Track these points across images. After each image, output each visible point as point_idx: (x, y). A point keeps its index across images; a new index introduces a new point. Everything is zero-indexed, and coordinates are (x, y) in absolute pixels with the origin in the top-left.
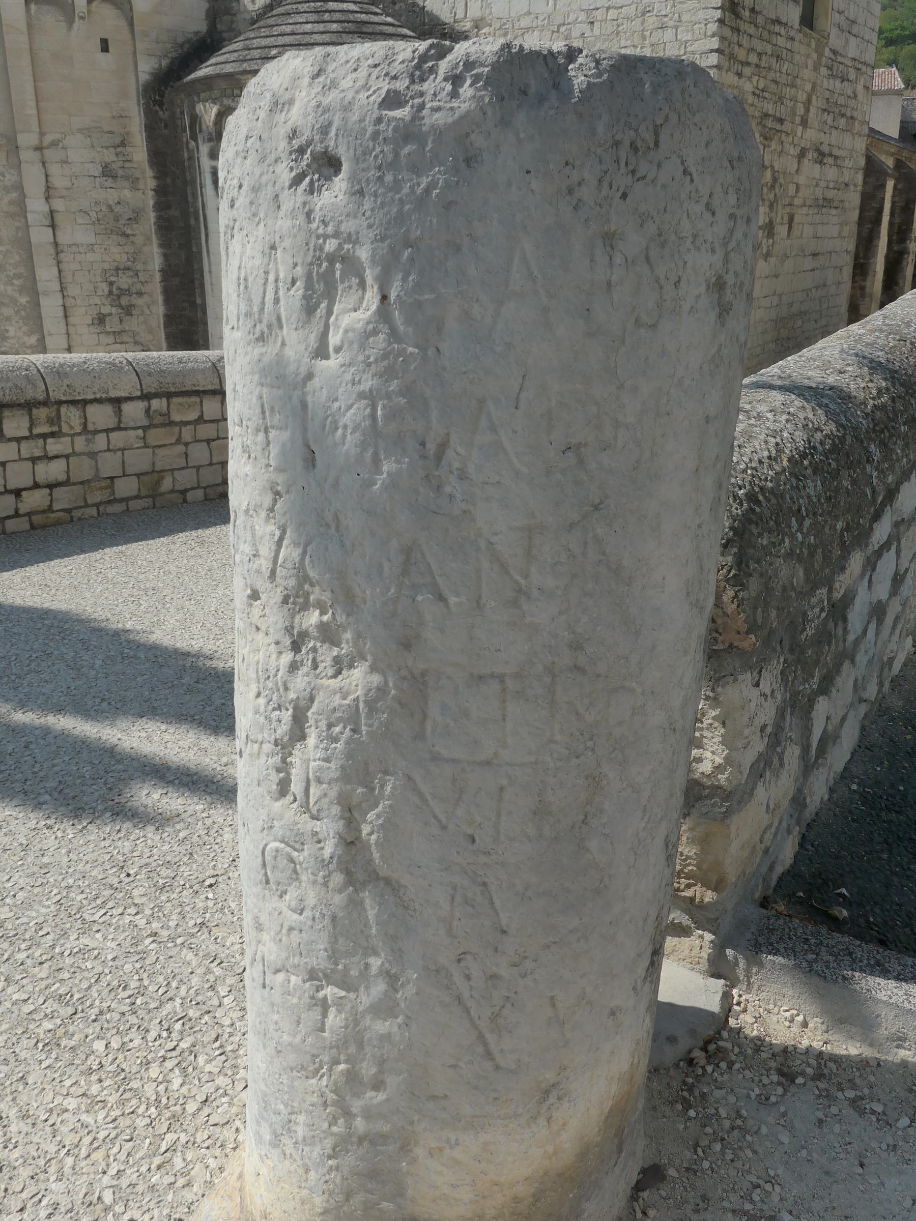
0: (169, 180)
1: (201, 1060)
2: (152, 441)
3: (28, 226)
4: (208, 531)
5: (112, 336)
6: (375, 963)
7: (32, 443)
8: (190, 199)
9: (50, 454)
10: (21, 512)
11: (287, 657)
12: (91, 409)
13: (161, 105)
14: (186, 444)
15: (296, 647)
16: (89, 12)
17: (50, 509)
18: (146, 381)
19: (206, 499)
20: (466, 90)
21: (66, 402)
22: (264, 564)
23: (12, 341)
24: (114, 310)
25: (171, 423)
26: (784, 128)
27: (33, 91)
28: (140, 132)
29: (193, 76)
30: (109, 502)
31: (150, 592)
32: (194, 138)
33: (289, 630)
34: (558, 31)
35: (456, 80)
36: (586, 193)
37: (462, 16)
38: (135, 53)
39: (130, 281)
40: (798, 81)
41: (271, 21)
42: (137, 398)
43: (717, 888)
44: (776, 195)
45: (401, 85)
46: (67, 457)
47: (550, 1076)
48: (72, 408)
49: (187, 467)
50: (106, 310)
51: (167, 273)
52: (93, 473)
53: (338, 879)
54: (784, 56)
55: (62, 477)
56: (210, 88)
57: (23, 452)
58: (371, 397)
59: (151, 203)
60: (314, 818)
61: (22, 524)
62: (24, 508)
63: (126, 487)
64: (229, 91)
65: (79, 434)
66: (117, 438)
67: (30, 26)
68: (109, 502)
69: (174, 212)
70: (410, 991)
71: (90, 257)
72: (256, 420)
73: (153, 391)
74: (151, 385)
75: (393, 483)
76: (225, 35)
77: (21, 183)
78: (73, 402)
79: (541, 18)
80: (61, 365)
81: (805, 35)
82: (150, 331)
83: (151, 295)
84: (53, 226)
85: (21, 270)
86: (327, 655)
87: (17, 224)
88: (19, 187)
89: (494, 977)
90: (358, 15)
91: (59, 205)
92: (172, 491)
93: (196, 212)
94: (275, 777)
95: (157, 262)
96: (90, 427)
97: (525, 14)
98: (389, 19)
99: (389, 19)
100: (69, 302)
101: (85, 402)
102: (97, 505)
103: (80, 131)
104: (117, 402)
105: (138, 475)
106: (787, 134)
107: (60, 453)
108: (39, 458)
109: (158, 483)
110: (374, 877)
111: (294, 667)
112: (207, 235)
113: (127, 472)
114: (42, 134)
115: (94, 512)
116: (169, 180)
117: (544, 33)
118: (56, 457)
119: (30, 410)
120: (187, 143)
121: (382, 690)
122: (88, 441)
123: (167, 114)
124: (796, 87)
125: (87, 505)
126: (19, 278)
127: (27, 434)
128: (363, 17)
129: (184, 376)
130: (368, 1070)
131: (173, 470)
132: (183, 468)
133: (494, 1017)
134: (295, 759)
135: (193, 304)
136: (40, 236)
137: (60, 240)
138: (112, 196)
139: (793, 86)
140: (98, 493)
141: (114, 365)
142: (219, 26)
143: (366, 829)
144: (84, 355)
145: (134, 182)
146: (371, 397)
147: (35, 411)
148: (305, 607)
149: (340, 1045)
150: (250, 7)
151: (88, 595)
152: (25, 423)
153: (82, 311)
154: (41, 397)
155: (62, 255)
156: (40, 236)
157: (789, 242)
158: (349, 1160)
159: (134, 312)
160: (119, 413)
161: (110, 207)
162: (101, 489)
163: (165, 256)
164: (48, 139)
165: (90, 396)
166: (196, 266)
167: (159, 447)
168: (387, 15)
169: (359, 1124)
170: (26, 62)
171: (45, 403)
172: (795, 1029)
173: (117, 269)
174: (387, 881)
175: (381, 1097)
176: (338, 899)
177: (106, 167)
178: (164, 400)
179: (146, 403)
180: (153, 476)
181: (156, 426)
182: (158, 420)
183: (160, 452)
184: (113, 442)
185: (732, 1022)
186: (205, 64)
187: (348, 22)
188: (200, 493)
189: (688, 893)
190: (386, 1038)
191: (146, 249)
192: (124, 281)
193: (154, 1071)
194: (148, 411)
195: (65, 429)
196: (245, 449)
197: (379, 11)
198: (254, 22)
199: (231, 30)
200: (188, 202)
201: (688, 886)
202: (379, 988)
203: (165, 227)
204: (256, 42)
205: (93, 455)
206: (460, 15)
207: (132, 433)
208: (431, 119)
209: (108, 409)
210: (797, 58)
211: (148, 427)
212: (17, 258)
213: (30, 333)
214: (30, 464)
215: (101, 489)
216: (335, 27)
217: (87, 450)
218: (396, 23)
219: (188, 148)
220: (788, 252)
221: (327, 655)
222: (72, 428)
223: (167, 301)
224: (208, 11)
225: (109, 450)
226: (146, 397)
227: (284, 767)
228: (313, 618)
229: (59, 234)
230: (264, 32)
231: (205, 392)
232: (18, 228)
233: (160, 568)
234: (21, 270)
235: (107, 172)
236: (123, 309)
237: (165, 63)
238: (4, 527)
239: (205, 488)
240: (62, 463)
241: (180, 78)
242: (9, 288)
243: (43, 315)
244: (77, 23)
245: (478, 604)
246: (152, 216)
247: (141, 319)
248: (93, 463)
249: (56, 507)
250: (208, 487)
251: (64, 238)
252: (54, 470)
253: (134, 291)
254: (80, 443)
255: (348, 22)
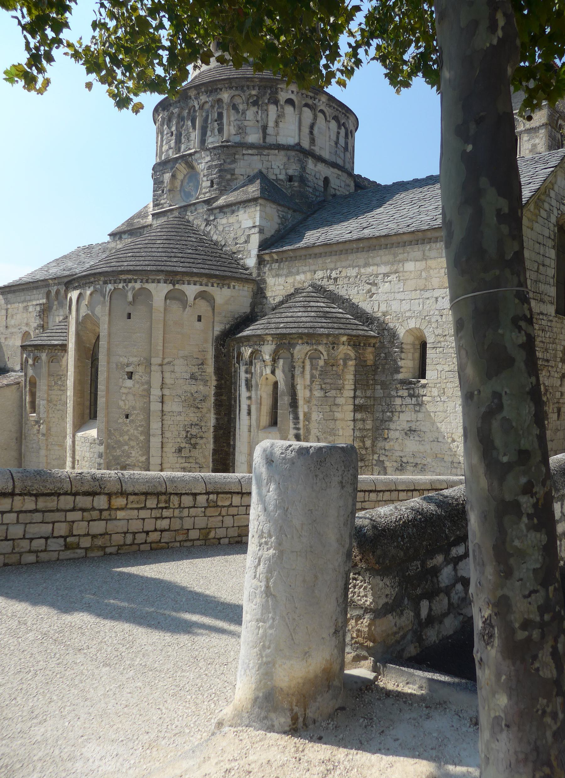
0: (223, 382)
1: (220, 702)
2: (208, 514)
3: (150, 402)
4: (230, 557)
5: (184, 459)
6: (270, 615)
7: (157, 511)
8: (233, 391)
9: (164, 516)
10: (148, 541)
11: (258, 548)
12: (183, 497)
13: (223, 346)
14: (223, 516)
15: (260, 546)
16: (194, 303)
17: (160, 541)
18: (209, 486)
19: (229, 543)
20: (293, 453)
21: (174, 494)
22: (256, 530)
23: (133, 459)
24: (187, 445)
25: (217, 506)
26: (549, 364)
27: (162, 339)
28: (212, 358)
29: (240, 335)
30: (186, 541)
31: (204, 578)
32: (238, 362)
33: (259, 542)
34: (425, 319)
35: (292, 451)
36: (312, 469)
37: (377, 310)
38: (214, 322)
39: (197, 431)
40: (557, 341)
41: (281, 310)
42: (204, 494)
43: (374, 642)
44: (547, 398)
45: (284, 451)
46: (170, 518)
47: (307, 649)
48: (176, 497)
49: (222, 527)
50: (183, 445)
51: (217, 428)
52: (180, 526)
53: (264, 595)
54: (547, 329)
55: (167, 527)
56: (249, 341)
57: (152, 514)
58: (276, 500)
59: (213, 392)
60: (261, 582)
61: (146, 547)
62: (149, 540)
63: (194, 534)
64: (258, 343)
65: (177, 508)
66: (193, 511)
67: (165, 309)
68: (186, 541)
69: (224, 398)
70: (277, 622)
71: (179, 418)
72: (257, 503)
73: (211, 491)
74: (210, 488)
75: (279, 515)
76: (259, 314)
77: (150, 381)
78: (176, 494)
79: (416, 312)
80: (173, 477)
81: (559, 318)
82: (205, 457)
83: (207, 439)
84: (162, 402)
85: (143, 423)
86: (266, 547)
87: (145, 400)
88: (149, 383)
89: (294, 619)
90: (325, 309)
91: (166, 392)
92: (214, 538)
93: (235, 398)
94: (254, 574)
95: (212, 422)
96: (182, 506)
97: (408, 310)
98: (341, 310)
99: (341, 310)
100: (165, 440)
101: (181, 494)
102: (180, 542)
103: (182, 357)
104: (195, 495)
105: (200, 529)
106: (552, 367)
107: (168, 516)
108: (159, 518)
109: (208, 534)
110: (271, 594)
111: (259, 550)
112: (240, 410)
113: (195, 527)
114: (163, 358)
115: (178, 544)
116: (223, 382)
117: (418, 319)
118: (166, 518)
119: (158, 496)
120: (234, 364)
121: (275, 554)
122: (180, 512)
123: (226, 350)
124: (556, 343)
125: (175, 541)
126: (142, 427)
127: (156, 507)
128: (328, 309)
129: (226, 485)
130: (267, 644)
131: (215, 528)
132: (220, 528)
133: (294, 629)
134: (258, 570)
135: (229, 445)
136: (155, 407)
137: (165, 409)
138: (194, 389)
139: (553, 343)
140: (181, 536)
141: (196, 478)
142: (256, 310)
143: (270, 583)
144: (183, 473)
145: (205, 382)
146: (276, 500)
147: (160, 497)
148: (262, 538)
149: (261, 638)
150: (272, 302)
151: (178, 577)
152: (155, 502)
153: (171, 445)
154: (164, 491)
155: (164, 417)
156: (155, 407)
157: (558, 422)
158: (262, 671)
159: (197, 447)
160: (195, 500)
161: (192, 394)
162: (183, 534)
163: (217, 419)
164: (166, 361)
165: (184, 492)
166: (232, 425)
167: (211, 517)
168: (339, 308)
169: (264, 659)
170: (161, 326)
171: (165, 494)
172: (395, 687)
173: (192, 425)
174: (274, 595)
175: (270, 651)
176: (264, 600)
177: (193, 374)
178: (215, 495)
179: (207, 496)
180: (206, 531)
181: (210, 507)
182: (212, 504)
183: (211, 519)
184: (190, 513)
185: (376, 683)
186: (247, 329)
187: (320, 312)
188: (227, 540)
189: (366, 644)
190: (271, 634)
191: (208, 415)
192: (194, 431)
193: (206, 703)
194: (207, 500)
195: (171, 506)
196: (254, 508)
197: (336, 306)
198: (274, 309)
199: (262, 312)
200: (231, 392)
201: (366, 642)
202: (271, 621)
203: (218, 405)
204: (273, 320)
205: (181, 518)
206: (376, 309)
207: (199, 509)
208: (288, 457)
209: (191, 498)
210: (555, 330)
211: (207, 507)
212: (142, 417)
213: (142, 455)
214: (155, 520)
215: (183, 534)
216: (313, 314)
217: (179, 515)
218: (344, 312)
219: (234, 366)
220: (559, 428)
221: (266, 547)
222: (174, 505)
223: (215, 442)
224: (251, 303)
225: (188, 516)
226: (208, 493)
227: (255, 572)
228: (264, 540)
229: (164, 406)
230: (278, 315)
231: (234, 493)
232: (145, 403)
233: (208, 569)
234: (143, 423)
235: (193, 377)
236: (192, 445)
237: (227, 326)
238: (139, 548)
239: (229, 538)
240: (168, 520)
241: (235, 334)
242: (136, 432)
243: (151, 446)
244: (188, 308)
245: (293, 537)
246: (212, 399)
247: (201, 451)
248: (181, 522)
249: (162, 541)
250: (231, 537)
251: (166, 409)
252: (164, 524)
253: (199, 436)
254: (177, 512)
255: (320, 312)
